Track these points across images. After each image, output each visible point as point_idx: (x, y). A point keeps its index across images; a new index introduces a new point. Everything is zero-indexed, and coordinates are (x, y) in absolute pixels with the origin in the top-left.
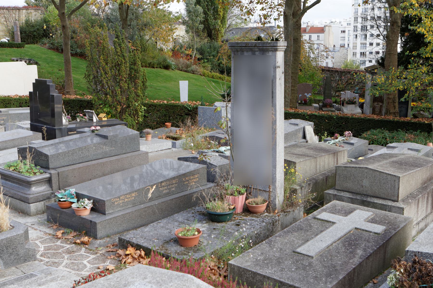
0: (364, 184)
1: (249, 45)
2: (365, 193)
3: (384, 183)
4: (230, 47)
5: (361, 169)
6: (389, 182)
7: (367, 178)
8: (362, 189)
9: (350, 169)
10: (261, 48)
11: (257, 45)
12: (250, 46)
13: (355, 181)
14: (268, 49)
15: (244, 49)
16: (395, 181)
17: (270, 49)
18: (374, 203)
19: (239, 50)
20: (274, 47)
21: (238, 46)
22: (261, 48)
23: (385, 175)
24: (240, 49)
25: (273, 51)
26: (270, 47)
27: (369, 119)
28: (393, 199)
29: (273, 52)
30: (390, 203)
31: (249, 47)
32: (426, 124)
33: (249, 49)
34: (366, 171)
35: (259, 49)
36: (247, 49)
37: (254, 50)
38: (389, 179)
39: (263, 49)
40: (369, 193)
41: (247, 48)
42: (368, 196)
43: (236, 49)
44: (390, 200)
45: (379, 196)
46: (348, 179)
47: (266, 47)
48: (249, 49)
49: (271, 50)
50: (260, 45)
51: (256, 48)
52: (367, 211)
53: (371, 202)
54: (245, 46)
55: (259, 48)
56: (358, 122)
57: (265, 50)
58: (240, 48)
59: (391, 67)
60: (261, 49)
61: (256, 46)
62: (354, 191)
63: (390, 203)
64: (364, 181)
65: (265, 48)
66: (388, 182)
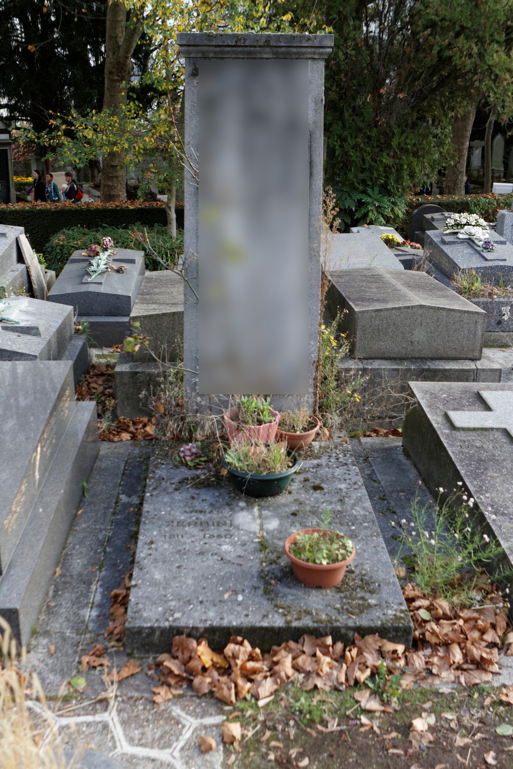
0: (415, 338)
1: (247, 43)
2: (417, 355)
3: (455, 331)
4: (185, 48)
5: (409, 310)
6: (465, 326)
7: (421, 325)
8: (410, 348)
9: (386, 313)
10: (284, 49)
11: (273, 43)
12: (247, 46)
13: (397, 336)
14: (304, 54)
15: (228, 53)
16: (476, 322)
17: (311, 53)
18: (445, 370)
19: (211, 55)
20: (321, 50)
21: (214, 43)
22: (284, 49)
23: (459, 315)
24: (215, 53)
25: (314, 59)
26: (309, 50)
27: (40, 210)
28: (471, 356)
29: (315, 62)
30: (471, 366)
31: (246, 49)
32: (132, 210)
33: (242, 53)
34: (420, 312)
35: (276, 53)
36: (237, 53)
37: (259, 56)
38: (465, 321)
39: (288, 53)
40: (427, 353)
41: (240, 49)
42: (424, 359)
43: (203, 53)
44: (466, 359)
45: (445, 356)
46: (381, 333)
47: (299, 50)
48: (242, 53)
49: (309, 56)
50: (282, 44)
51: (268, 49)
52: (496, 389)
53: (440, 370)
54: (234, 43)
55: (275, 50)
56: (24, 218)
57: (293, 56)
58: (218, 49)
59: (89, 110)
60: (282, 53)
61: (268, 46)
62: (395, 356)
63: (471, 366)
64: (416, 332)
65: (294, 50)
66: (463, 327)
